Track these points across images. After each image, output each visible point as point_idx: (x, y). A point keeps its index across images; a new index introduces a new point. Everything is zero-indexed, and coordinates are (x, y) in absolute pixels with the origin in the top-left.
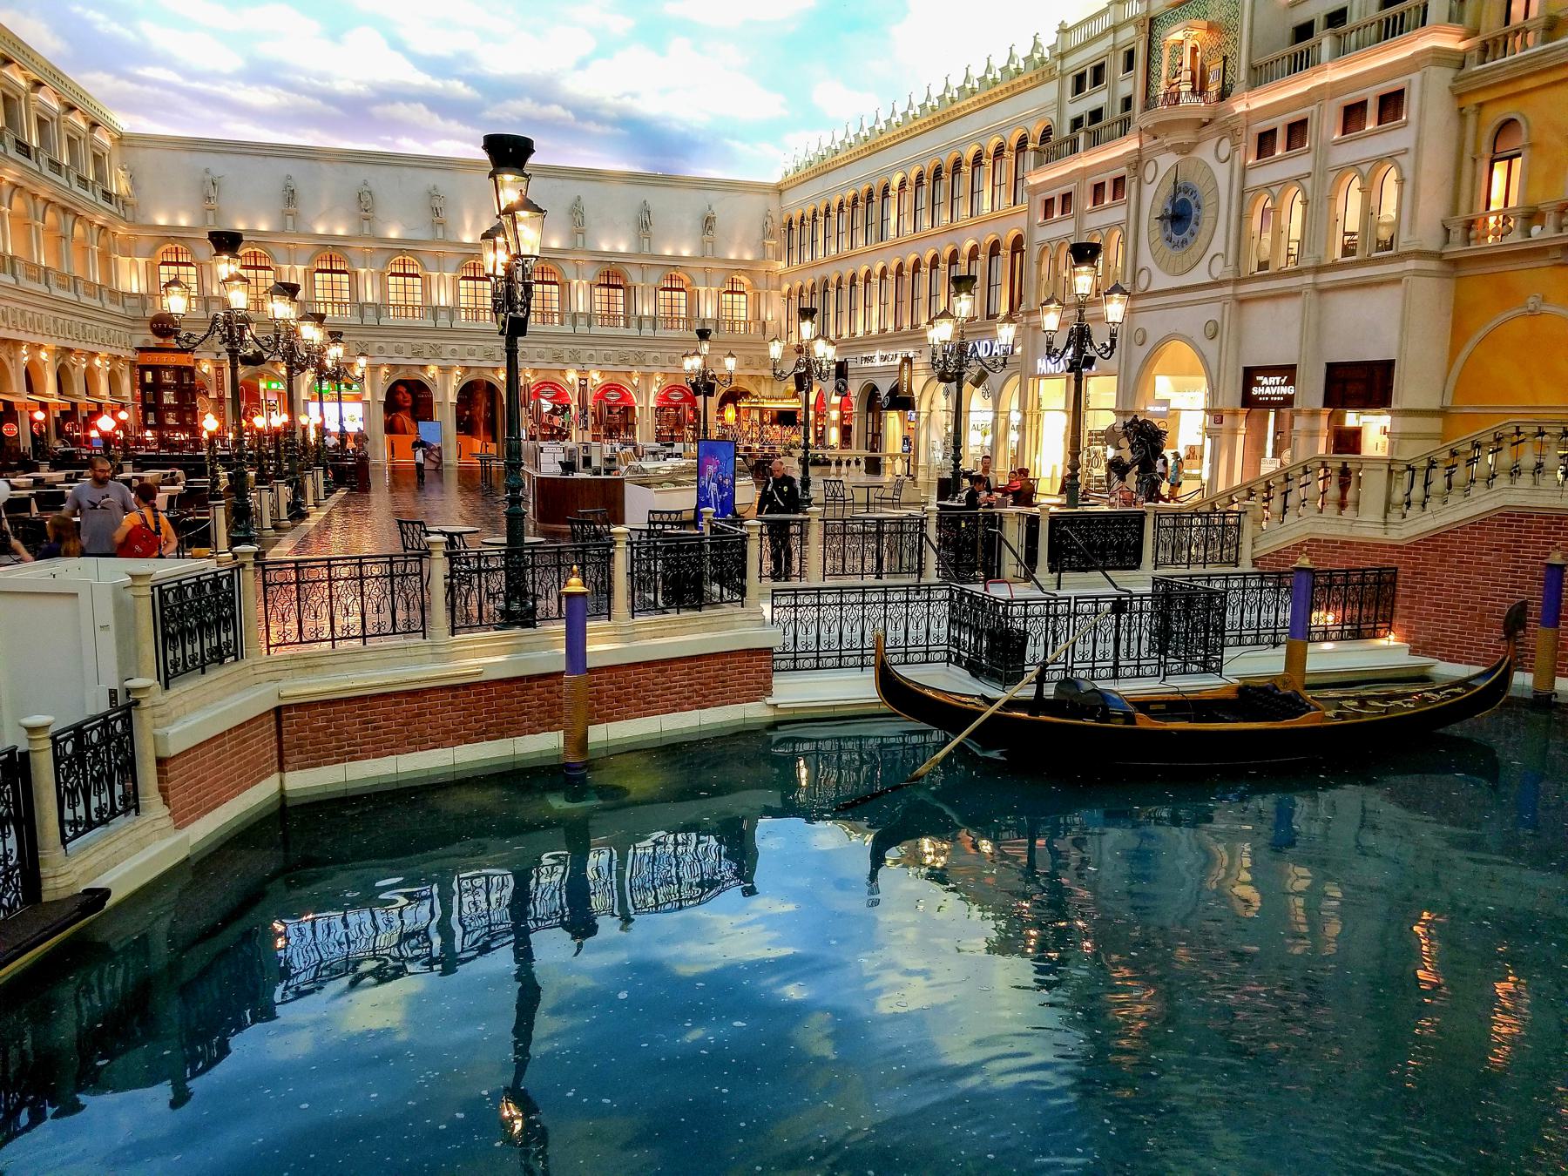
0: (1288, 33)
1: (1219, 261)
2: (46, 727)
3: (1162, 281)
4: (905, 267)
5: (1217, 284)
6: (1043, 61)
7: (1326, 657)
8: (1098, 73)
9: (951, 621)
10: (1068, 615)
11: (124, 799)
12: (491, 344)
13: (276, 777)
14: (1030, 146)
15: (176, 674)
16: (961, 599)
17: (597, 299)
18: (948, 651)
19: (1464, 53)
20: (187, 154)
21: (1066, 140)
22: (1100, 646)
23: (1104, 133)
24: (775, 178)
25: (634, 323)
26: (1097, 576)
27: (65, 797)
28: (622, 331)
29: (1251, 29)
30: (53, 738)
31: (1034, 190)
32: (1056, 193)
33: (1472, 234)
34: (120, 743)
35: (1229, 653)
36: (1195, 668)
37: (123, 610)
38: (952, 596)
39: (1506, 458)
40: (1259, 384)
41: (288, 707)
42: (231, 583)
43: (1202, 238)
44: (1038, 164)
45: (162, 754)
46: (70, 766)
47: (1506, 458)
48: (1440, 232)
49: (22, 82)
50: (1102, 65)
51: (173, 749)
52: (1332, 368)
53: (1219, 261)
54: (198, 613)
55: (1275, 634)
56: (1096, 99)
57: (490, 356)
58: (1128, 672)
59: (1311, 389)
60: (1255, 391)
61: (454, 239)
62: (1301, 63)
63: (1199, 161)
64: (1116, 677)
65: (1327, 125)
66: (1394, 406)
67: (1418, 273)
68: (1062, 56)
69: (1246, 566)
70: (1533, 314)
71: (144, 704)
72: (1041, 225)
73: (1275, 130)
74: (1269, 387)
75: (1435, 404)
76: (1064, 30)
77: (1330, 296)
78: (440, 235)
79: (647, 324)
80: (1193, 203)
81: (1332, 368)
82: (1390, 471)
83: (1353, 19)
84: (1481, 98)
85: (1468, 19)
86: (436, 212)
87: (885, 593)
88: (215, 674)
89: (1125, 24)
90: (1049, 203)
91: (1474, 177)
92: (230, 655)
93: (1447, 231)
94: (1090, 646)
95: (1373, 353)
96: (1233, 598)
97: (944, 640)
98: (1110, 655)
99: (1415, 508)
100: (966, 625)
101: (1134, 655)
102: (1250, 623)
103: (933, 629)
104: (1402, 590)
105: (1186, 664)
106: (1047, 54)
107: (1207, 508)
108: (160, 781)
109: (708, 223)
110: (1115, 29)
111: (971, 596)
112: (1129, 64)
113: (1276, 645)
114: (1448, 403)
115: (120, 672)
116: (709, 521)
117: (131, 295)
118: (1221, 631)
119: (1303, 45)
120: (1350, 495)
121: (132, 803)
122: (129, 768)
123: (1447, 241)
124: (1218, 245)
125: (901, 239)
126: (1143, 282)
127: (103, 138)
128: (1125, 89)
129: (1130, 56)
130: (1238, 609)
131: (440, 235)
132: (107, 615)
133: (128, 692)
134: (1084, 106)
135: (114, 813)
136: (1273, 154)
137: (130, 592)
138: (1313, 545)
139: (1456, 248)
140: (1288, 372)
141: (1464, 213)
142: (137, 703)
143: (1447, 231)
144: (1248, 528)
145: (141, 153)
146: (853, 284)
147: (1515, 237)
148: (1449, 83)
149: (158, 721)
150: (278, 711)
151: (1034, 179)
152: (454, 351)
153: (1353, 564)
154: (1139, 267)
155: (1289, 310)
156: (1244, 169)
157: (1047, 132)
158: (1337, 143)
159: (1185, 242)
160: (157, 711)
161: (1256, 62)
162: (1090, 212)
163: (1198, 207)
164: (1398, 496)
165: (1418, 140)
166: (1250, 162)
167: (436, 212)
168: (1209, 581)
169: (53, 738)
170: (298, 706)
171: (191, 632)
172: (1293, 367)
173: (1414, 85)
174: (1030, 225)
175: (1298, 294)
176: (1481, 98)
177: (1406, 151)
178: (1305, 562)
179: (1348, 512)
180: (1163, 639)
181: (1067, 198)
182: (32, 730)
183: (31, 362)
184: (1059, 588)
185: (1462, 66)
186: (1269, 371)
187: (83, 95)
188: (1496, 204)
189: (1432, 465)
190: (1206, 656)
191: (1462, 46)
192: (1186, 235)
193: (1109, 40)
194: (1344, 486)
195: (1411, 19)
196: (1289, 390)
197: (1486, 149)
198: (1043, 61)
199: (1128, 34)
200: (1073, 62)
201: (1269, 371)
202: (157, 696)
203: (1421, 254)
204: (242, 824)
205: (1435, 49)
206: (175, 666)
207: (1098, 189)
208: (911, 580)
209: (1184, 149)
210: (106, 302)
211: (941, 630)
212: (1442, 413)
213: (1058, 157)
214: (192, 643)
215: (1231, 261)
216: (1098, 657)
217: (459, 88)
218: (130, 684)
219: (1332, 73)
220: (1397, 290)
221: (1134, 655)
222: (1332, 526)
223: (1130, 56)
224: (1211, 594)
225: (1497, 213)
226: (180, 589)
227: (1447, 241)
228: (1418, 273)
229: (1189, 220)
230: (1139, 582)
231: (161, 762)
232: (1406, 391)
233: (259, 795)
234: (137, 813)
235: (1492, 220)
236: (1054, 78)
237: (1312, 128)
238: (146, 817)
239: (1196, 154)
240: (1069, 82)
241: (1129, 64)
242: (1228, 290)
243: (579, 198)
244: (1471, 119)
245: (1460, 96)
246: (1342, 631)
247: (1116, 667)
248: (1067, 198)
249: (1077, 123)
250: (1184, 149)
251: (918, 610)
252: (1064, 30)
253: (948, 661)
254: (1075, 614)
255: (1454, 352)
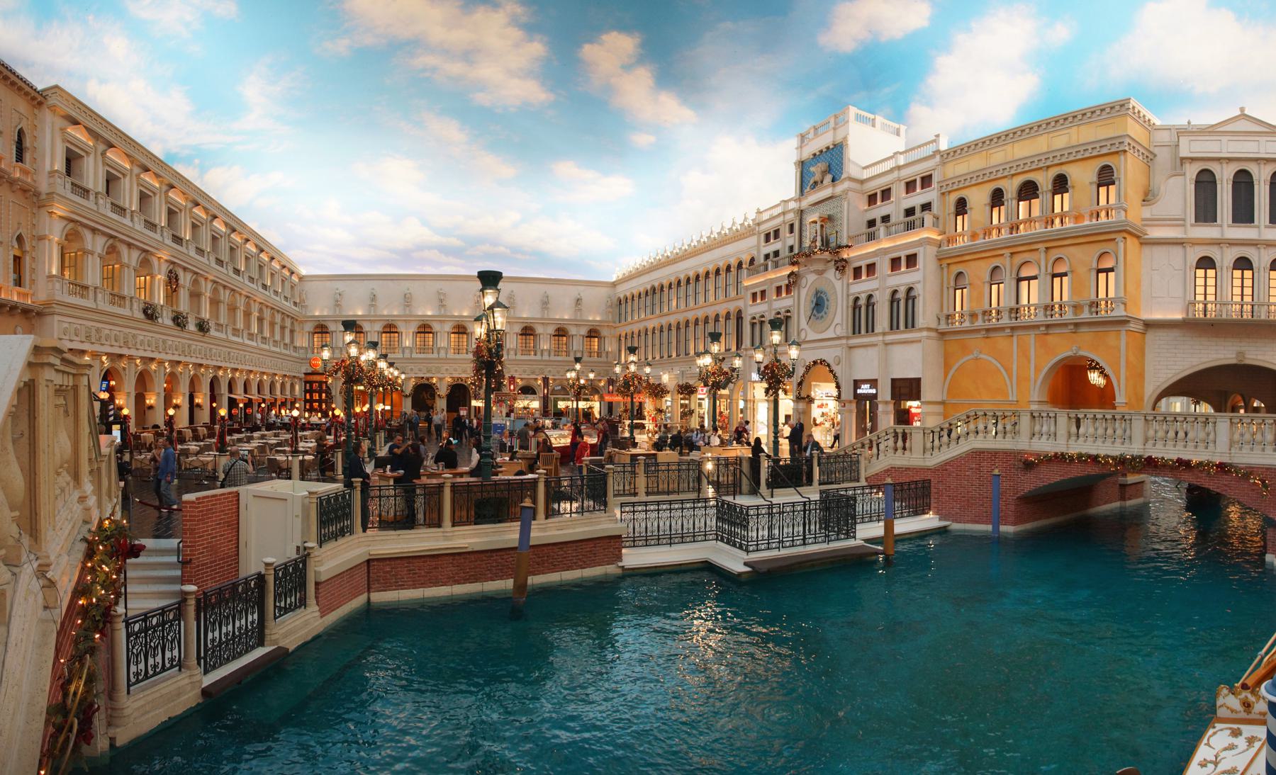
0: (865, 224)
1: (839, 328)
2: (273, 564)
3: (812, 336)
4: (681, 324)
5: (839, 338)
6: (749, 226)
7: (903, 526)
8: (777, 233)
9: (717, 518)
10: (780, 513)
11: (300, 600)
12: (465, 365)
13: (365, 595)
14: (744, 266)
15: (325, 541)
16: (722, 505)
17: (452, 340)
18: (716, 534)
19: (941, 241)
20: (329, 282)
21: (762, 265)
22: (796, 529)
23: (780, 262)
24: (614, 279)
25: (539, 353)
26: (791, 490)
27: (277, 596)
28: (532, 357)
29: (848, 220)
30: (275, 569)
31: (747, 288)
32: (758, 290)
33: (950, 321)
34: (301, 573)
35: (858, 527)
36: (843, 536)
37: (305, 509)
38: (717, 504)
39: (972, 426)
40: (860, 388)
41: (374, 560)
42: (350, 496)
43: (830, 316)
44: (749, 275)
45: (318, 580)
46: (280, 583)
47: (972, 426)
48: (936, 319)
49: (267, 259)
50: (779, 230)
51: (323, 578)
52: (894, 381)
53: (839, 327)
54: (335, 511)
55: (879, 516)
56: (774, 246)
57: (465, 372)
58: (810, 541)
59: (885, 393)
60: (859, 391)
61: (449, 314)
62: (871, 237)
63: (826, 278)
64: (804, 544)
65: (884, 266)
66: (922, 400)
67: (928, 338)
68: (759, 224)
69: (863, 483)
70: (977, 359)
71: (312, 555)
72: (751, 306)
73: (861, 267)
74: (865, 389)
75: (940, 400)
76: (759, 212)
77: (890, 347)
78: (443, 312)
79: (546, 354)
80: (825, 298)
81: (894, 381)
82: (924, 433)
83: (893, 220)
84: (949, 261)
85: (941, 226)
86: (441, 301)
87: (682, 504)
88: (341, 541)
89: (789, 211)
90: (754, 295)
91: (948, 294)
92: (348, 532)
93: (939, 319)
94: (791, 530)
95: (912, 375)
96: (859, 499)
97: (714, 528)
98: (801, 533)
99: (936, 450)
100: (738, 524)
101: (813, 532)
102: (867, 511)
103: (708, 522)
104: (933, 490)
105: (838, 535)
106: (751, 223)
107: (843, 453)
108: (316, 593)
109: (374, 298)
110: (784, 213)
111: (728, 505)
112: (791, 231)
113: (879, 521)
114: (945, 398)
115: (302, 537)
116: (586, 465)
117: (302, 348)
118: (854, 517)
119: (872, 230)
120: (908, 445)
121: (303, 603)
122: (302, 585)
123: (939, 324)
124: (838, 320)
125: (697, 306)
126: (803, 335)
127: (295, 278)
128: (790, 242)
129: (792, 226)
130: (869, 504)
131: (443, 312)
132: (298, 511)
133: (305, 548)
134: (770, 248)
135: (296, 607)
136: (861, 278)
137: (308, 499)
138: (890, 471)
139: (943, 327)
140: (873, 383)
141: (945, 312)
142: (309, 554)
143: (939, 319)
144: (863, 463)
145: (309, 283)
146: (653, 333)
147: (967, 324)
148: (936, 253)
149: (317, 564)
150: (368, 561)
151: (746, 284)
152: (447, 370)
153: (897, 482)
154: (801, 328)
155: (872, 352)
156: (848, 285)
157: (752, 261)
158: (889, 276)
159: (822, 317)
160: (317, 559)
161: (850, 234)
162: (775, 300)
163: (828, 300)
164: (929, 445)
165: (924, 278)
166: (851, 281)
167: (441, 301)
168: (846, 491)
169: (275, 569)
170: (378, 560)
171: (332, 520)
172: (876, 380)
173: (920, 252)
174: (746, 305)
175: (875, 345)
176: (949, 261)
177: (919, 282)
178: (889, 480)
179: (907, 453)
180: (825, 524)
181: (763, 292)
182: (267, 564)
183: (195, 375)
184: (772, 497)
185: (940, 247)
186: (865, 382)
187: (288, 261)
188: (958, 308)
189: (942, 429)
190: (848, 530)
191: (939, 238)
192: (823, 313)
193: (781, 219)
194: (904, 440)
195: (917, 223)
196: (874, 391)
197: (952, 283)
198: (749, 226)
199: (790, 216)
200: (764, 227)
201: (865, 382)
202: (315, 553)
203: (929, 329)
204: (333, 624)
205: (928, 238)
206: (325, 536)
207: (779, 289)
208: (693, 496)
209: (820, 273)
210: (260, 343)
211: (712, 523)
212: (943, 403)
213: (758, 272)
214: (332, 525)
215: (844, 325)
216: (795, 534)
217: (454, 242)
218: (306, 545)
219: (886, 244)
220: (919, 346)
221: (813, 532)
222: (900, 460)
223: (792, 226)
224: (848, 498)
225: (958, 312)
226: (329, 499)
227: (939, 324)
228: (928, 338)
229: (823, 307)
230: (813, 493)
231: (317, 584)
232: (928, 392)
233: (358, 602)
234: (305, 608)
235: (957, 315)
236: (754, 234)
237: (878, 267)
238: (309, 610)
239: (825, 275)
240: (763, 237)
241: (791, 231)
242: (844, 341)
243: (512, 291)
244: (945, 269)
245: (940, 260)
246: (909, 512)
247: (804, 539)
248: (763, 292)
249: (767, 256)
250: (820, 273)
251: (700, 512)
252: (759, 212)
253: (717, 539)
254: (783, 512)
255: (945, 377)
